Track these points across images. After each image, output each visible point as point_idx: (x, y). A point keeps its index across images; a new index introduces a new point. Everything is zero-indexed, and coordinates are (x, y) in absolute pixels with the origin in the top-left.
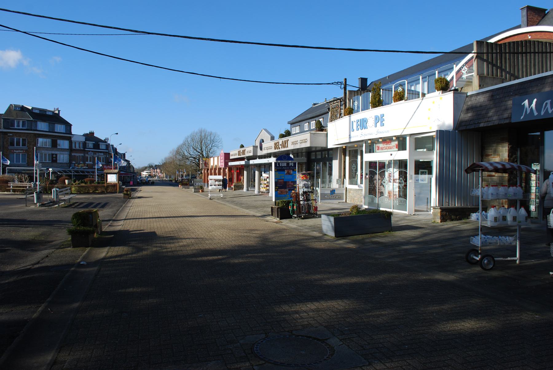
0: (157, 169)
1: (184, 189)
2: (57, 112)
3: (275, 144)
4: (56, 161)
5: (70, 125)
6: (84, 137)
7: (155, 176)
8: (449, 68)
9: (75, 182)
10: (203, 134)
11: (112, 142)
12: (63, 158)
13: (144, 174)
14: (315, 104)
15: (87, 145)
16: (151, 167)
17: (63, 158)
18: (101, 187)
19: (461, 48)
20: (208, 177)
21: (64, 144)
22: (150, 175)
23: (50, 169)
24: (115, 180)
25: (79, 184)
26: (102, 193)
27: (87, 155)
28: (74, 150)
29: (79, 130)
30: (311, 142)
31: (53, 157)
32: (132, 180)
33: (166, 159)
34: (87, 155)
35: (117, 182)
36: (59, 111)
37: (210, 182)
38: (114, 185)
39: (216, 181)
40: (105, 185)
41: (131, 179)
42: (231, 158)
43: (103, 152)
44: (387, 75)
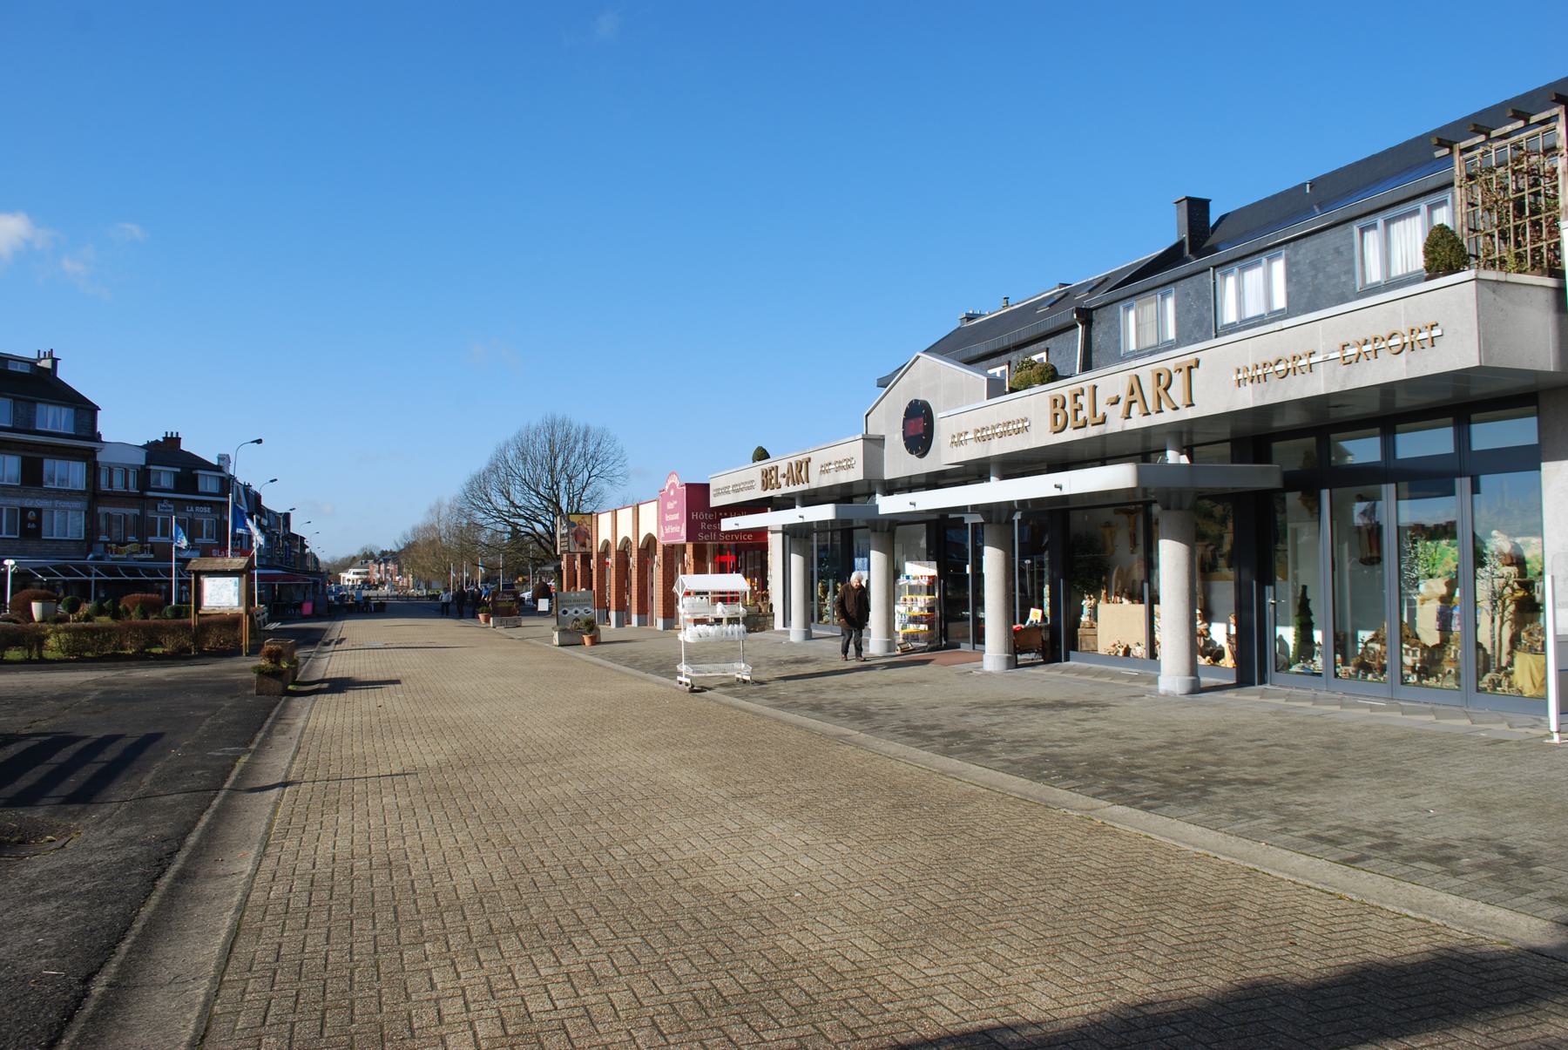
0: (386, 561)
1: (501, 629)
2: (46, 364)
3: (765, 474)
4: (37, 533)
5: (92, 410)
6: (144, 452)
7: (382, 583)
8: (1199, 268)
9: (73, 608)
10: (559, 435)
11: (244, 472)
12: (67, 523)
13: (349, 577)
14: (970, 318)
15: (153, 478)
16: (368, 557)
17: (67, 523)
18: (172, 632)
19: (1480, 113)
20: (669, 580)
21: (74, 474)
22: (365, 582)
23: (9, 562)
24: (235, 601)
25: (88, 618)
26: (179, 656)
27: (151, 514)
28: (106, 494)
29: (125, 426)
30: (1485, 342)
31: (24, 521)
32: (310, 596)
33: (415, 530)
34: (151, 514)
35: (242, 610)
36: (55, 361)
37: (684, 608)
38: (229, 623)
39: (715, 601)
40: (193, 620)
41: (298, 593)
42: (715, 502)
43: (210, 504)
44: (1307, 178)
